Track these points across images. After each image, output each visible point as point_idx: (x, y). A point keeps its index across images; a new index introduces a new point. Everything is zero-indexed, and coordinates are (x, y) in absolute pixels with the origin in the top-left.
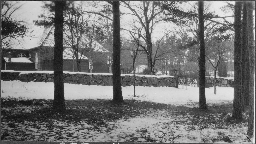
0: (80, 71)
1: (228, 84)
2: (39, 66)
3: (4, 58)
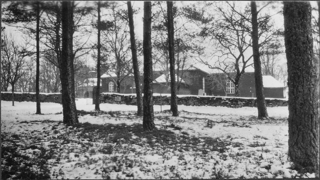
0: (119, 93)
1: (122, 101)
2: (233, 88)
3: (240, 72)
